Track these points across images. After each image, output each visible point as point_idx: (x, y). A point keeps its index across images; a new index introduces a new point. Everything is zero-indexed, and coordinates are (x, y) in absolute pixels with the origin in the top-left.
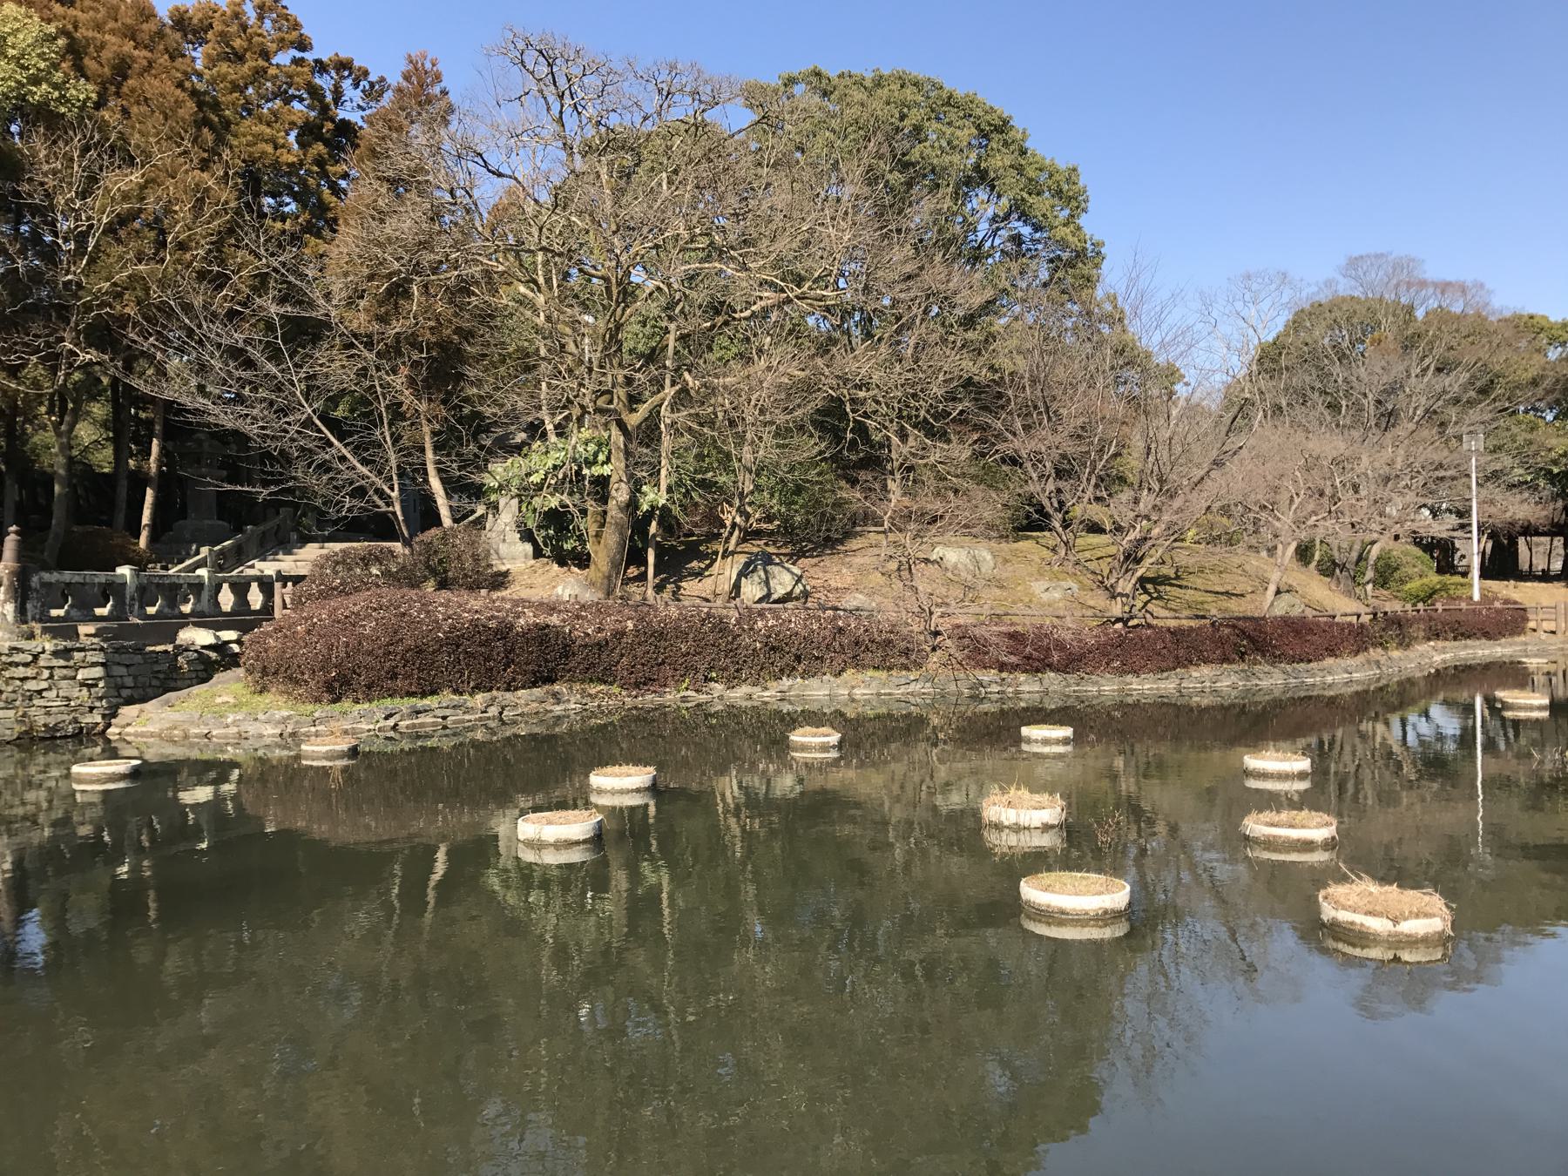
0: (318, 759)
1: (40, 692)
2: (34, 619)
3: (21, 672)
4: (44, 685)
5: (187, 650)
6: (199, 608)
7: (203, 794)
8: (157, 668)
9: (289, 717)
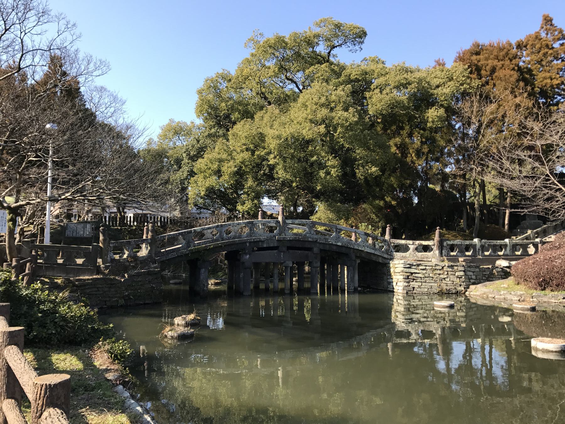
0: (518, 310)
1: (444, 279)
2: (445, 256)
3: (438, 272)
4: (445, 276)
5: (497, 267)
6: (506, 253)
7: (506, 319)
8: (484, 273)
9: (523, 294)
